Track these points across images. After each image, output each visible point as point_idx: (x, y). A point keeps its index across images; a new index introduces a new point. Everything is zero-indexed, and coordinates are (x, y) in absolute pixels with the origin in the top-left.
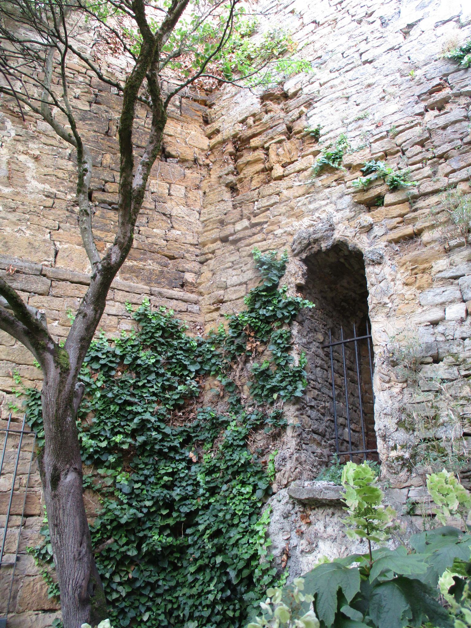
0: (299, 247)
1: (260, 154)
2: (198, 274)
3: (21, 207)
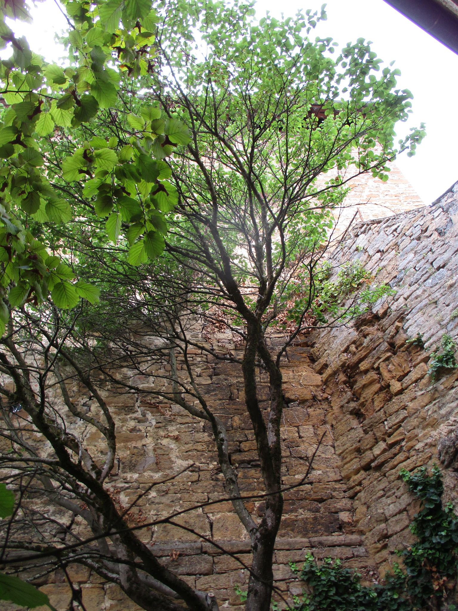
0: (447, 457)
1: (373, 375)
2: (352, 510)
3: (172, 488)
